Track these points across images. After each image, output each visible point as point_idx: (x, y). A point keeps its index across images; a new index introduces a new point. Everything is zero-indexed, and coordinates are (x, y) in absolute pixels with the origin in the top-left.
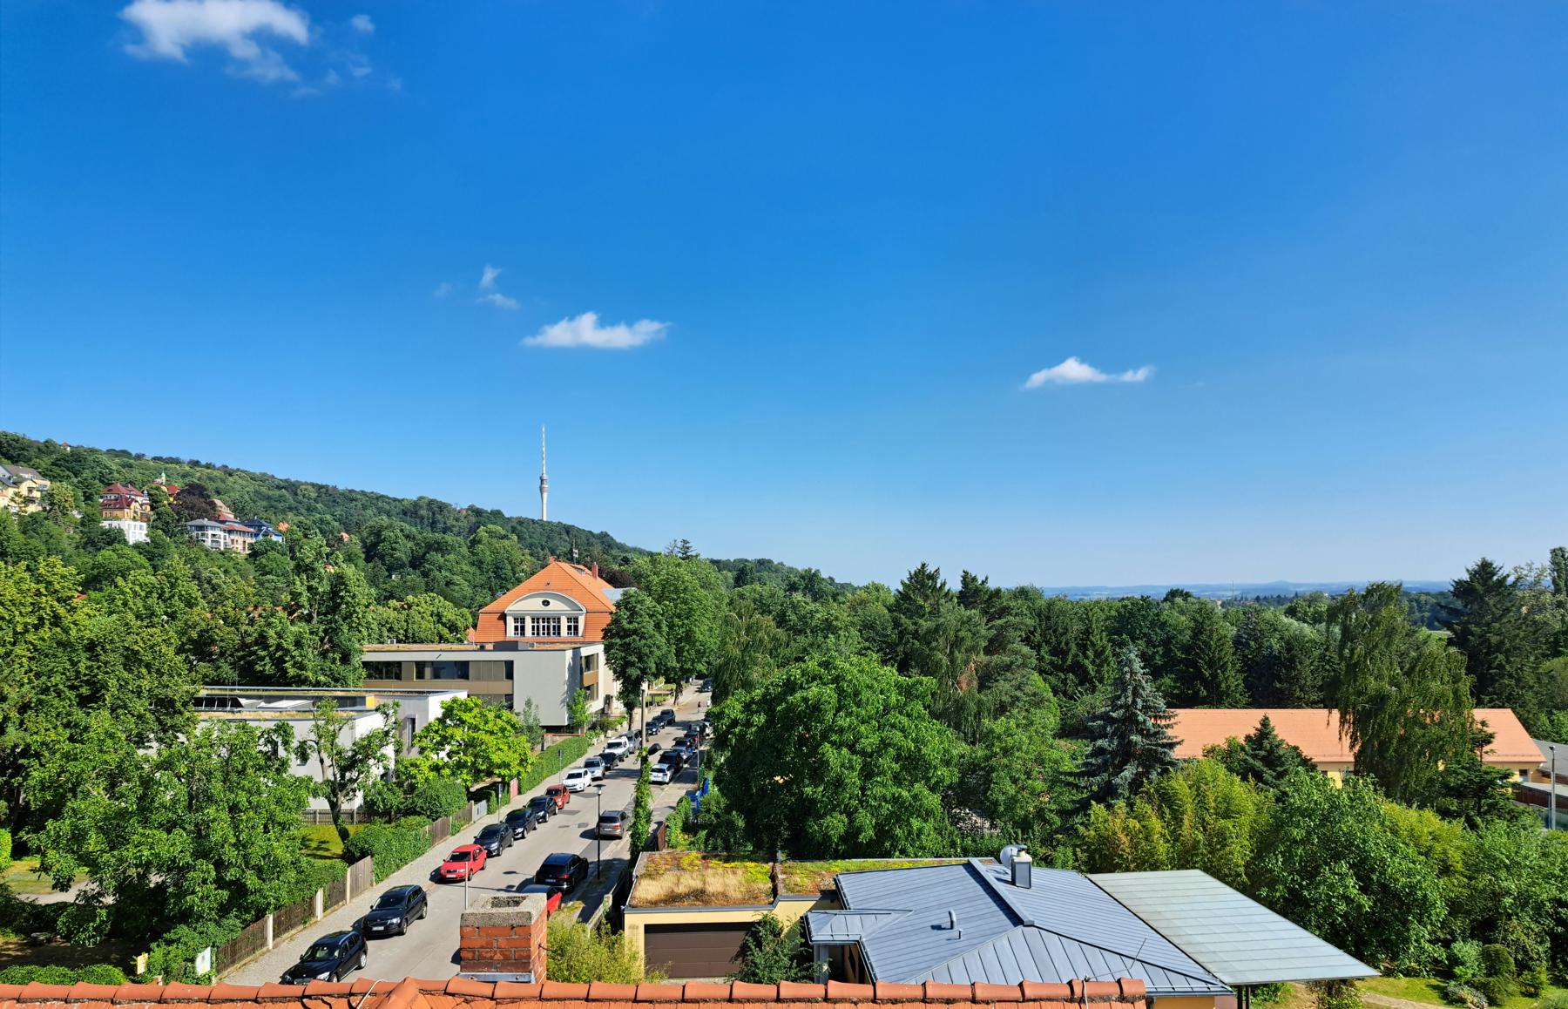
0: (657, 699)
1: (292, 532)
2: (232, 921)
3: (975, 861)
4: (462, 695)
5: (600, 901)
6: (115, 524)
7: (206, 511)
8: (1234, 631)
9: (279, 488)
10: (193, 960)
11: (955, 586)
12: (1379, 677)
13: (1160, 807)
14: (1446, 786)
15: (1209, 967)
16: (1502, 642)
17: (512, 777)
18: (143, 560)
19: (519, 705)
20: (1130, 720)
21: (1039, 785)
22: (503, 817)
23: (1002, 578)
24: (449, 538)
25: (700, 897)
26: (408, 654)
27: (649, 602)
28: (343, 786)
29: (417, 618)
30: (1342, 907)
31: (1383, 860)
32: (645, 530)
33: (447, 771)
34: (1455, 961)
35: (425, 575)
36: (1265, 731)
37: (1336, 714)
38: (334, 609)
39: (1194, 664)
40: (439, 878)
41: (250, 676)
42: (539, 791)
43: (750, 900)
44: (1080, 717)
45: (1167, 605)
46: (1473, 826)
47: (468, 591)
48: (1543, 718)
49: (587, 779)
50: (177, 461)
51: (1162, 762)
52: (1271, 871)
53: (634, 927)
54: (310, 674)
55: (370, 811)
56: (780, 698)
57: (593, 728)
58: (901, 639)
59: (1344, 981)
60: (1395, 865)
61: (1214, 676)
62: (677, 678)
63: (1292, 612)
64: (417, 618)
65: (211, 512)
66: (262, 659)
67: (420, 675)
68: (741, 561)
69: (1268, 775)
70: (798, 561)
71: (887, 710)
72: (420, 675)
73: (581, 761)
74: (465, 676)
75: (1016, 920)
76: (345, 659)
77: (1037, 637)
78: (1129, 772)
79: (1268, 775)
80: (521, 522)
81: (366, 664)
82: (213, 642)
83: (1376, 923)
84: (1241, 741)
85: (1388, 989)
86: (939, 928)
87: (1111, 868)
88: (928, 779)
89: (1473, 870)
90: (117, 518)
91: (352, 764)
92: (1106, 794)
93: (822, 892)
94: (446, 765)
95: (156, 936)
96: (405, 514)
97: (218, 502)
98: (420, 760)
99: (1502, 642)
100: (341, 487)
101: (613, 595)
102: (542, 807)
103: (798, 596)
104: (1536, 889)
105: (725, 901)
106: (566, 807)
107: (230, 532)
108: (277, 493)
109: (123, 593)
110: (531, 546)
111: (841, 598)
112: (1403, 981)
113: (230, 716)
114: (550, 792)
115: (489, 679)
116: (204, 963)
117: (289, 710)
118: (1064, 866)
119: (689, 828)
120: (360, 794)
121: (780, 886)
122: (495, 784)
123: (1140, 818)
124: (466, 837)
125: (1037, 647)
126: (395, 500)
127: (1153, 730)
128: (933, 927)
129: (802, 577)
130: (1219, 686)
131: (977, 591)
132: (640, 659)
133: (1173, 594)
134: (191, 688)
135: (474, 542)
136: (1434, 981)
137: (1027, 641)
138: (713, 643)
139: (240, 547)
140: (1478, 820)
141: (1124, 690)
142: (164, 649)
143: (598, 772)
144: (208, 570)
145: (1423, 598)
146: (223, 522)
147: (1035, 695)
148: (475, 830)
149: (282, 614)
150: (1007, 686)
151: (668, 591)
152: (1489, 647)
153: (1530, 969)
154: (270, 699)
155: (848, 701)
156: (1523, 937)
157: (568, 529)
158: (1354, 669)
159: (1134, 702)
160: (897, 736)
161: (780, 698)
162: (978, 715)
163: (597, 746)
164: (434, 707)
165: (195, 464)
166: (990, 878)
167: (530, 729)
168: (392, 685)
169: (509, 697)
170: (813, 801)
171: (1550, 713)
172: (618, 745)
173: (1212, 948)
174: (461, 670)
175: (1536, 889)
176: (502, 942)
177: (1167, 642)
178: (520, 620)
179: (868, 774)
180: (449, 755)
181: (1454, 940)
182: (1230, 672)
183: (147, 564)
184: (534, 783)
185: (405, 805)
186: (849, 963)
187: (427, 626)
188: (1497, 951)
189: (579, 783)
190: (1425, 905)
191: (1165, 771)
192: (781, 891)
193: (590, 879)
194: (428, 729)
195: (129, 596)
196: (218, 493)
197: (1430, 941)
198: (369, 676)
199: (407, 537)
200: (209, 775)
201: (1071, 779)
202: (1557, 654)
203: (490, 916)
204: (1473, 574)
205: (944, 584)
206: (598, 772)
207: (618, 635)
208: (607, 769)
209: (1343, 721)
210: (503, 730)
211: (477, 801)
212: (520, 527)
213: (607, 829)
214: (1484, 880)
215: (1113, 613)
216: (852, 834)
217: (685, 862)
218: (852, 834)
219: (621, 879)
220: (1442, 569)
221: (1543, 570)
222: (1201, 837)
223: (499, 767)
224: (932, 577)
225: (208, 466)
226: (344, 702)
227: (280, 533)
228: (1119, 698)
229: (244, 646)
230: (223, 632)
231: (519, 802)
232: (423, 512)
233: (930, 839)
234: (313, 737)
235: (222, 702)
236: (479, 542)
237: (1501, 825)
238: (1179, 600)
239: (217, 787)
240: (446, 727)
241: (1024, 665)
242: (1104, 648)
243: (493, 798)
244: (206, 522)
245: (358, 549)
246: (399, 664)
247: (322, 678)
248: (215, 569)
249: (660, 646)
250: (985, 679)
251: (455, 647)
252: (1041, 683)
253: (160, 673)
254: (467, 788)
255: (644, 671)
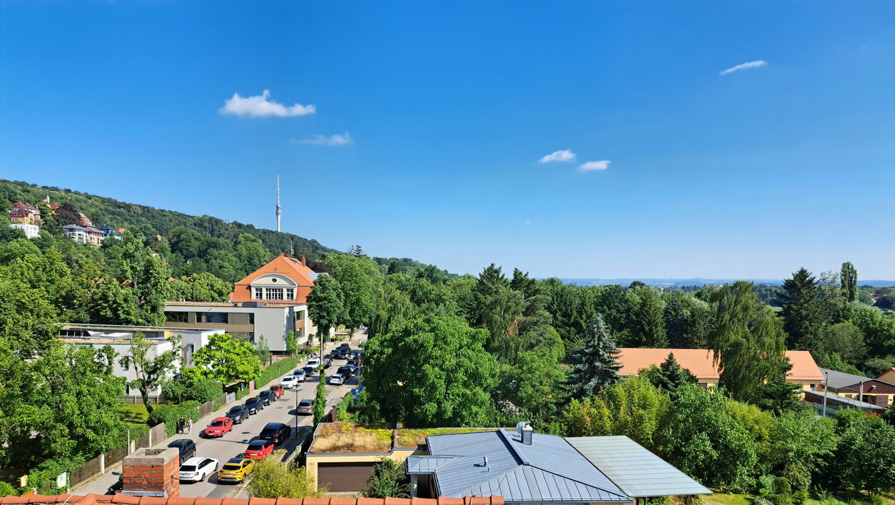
0: (339, 337)
1: (127, 234)
2: (79, 457)
3: (503, 430)
4: (221, 332)
5: (294, 449)
6: (19, 226)
7: (74, 220)
8: (664, 305)
9: (119, 207)
10: (55, 479)
11: (510, 277)
12: (737, 333)
13: (608, 402)
14: (765, 393)
15: (622, 487)
16: (808, 315)
17: (250, 380)
18: (36, 248)
19: (257, 339)
20: (595, 355)
21: (547, 389)
22: (244, 402)
23: (537, 272)
24: (222, 240)
25: (350, 448)
26: (193, 308)
27: (333, 281)
28: (149, 383)
29: (199, 287)
30: (702, 457)
31: (726, 432)
32: (336, 240)
33: (211, 376)
34: (760, 485)
35: (207, 261)
36: (670, 362)
37: (712, 352)
38: (147, 280)
39: (640, 323)
40: (204, 435)
41: (97, 318)
42: (266, 388)
43: (378, 449)
44: (569, 350)
45: (631, 290)
46: (778, 415)
47: (233, 272)
48: (827, 356)
49: (295, 382)
50: (56, 189)
51: (612, 378)
52: (666, 437)
53: (311, 464)
54: (133, 318)
55: (166, 397)
56: (401, 339)
57: (301, 353)
58: (478, 306)
59: (693, 496)
60: (732, 435)
61: (651, 330)
62: (352, 326)
63: (699, 295)
64: (199, 287)
65: (77, 220)
66: (105, 308)
67: (199, 320)
68: (393, 259)
69: (671, 385)
70: (424, 258)
71: (461, 348)
72: (199, 320)
73: (292, 372)
74: (226, 321)
75: (520, 461)
76: (154, 309)
77: (555, 307)
78: (593, 382)
79: (671, 385)
80: (265, 232)
81: (166, 313)
82: (75, 297)
83: (721, 465)
84: (659, 367)
85: (724, 500)
86: (478, 465)
87: (581, 434)
88: (481, 385)
89: (774, 438)
90: (20, 223)
91: (154, 370)
92: (580, 395)
93: (419, 446)
94: (211, 372)
95: (34, 465)
96: (195, 225)
97: (82, 215)
98: (195, 369)
99: (808, 315)
100: (157, 208)
101: (313, 276)
102: (267, 397)
103: (424, 281)
104: (807, 448)
105: (364, 450)
106: (282, 397)
107: (89, 233)
108: (118, 210)
109: (21, 267)
110: (270, 247)
111: (448, 283)
112: (732, 496)
113: (83, 341)
114: (272, 388)
115: (240, 323)
116: (62, 481)
117: (119, 341)
118: (554, 433)
119: (350, 410)
120: (159, 387)
121: (396, 442)
122: (240, 383)
123: (598, 407)
124: (221, 413)
125: (554, 313)
126: (189, 216)
127: (608, 360)
128: (475, 465)
129: (426, 270)
130: (653, 336)
131: (522, 280)
132: (328, 314)
133: (635, 284)
134: (59, 324)
135: (236, 243)
136: (748, 496)
137: (548, 308)
138: (372, 306)
139: (96, 242)
140: (781, 411)
141: (593, 337)
142: (41, 301)
143: (302, 378)
144: (76, 255)
145: (774, 289)
146: (85, 227)
147: (550, 339)
148: (227, 409)
149: (115, 282)
150: (535, 334)
151: (347, 275)
152: (801, 317)
153: (798, 489)
154: (107, 332)
155: (440, 342)
156: (797, 474)
157: (292, 237)
158: (722, 328)
159: (598, 344)
160: (467, 361)
161: (401, 339)
162: (517, 350)
163: (303, 363)
164: (204, 339)
165: (68, 191)
166: (509, 439)
167: (263, 353)
168: (182, 325)
169: (252, 335)
170: (419, 397)
171: (830, 354)
172: (314, 363)
173: (625, 477)
174: (224, 318)
175: (807, 448)
176: (147, 474)
177: (628, 311)
178: (259, 290)
179: (449, 382)
180: (213, 366)
181: (761, 475)
182: (660, 328)
183: (38, 250)
184: (264, 383)
185: (185, 393)
186: (427, 487)
187: (204, 291)
188: (782, 481)
189: (290, 384)
190: (746, 455)
191: (613, 382)
192: (396, 445)
193: (292, 437)
194: (200, 351)
195: (25, 269)
196: (82, 209)
197: (748, 475)
198: (169, 320)
199: (196, 239)
200: (63, 375)
201: (562, 386)
202: (838, 322)
203: (140, 460)
204: (796, 276)
205: (503, 276)
206: (302, 378)
207: (315, 299)
208: (307, 376)
209: (716, 356)
210: (244, 353)
211: (229, 392)
212: (265, 235)
213: (304, 409)
214: (779, 444)
215: (600, 294)
216: (440, 414)
217: (344, 428)
218: (440, 414)
219: (306, 437)
220: (779, 273)
221: (837, 275)
222: (629, 419)
223: (242, 374)
224: (497, 272)
225: (76, 193)
226: (149, 334)
227: (119, 235)
228: (590, 341)
229: (93, 300)
230: (80, 292)
231: (254, 393)
232: (206, 224)
233: (482, 417)
234: (131, 354)
235: (78, 333)
236: (240, 243)
237: (791, 414)
238: (638, 287)
239: (69, 382)
240: (210, 350)
241: (545, 323)
242: (592, 313)
243: (239, 391)
244: (74, 226)
245: (166, 245)
246: (187, 313)
247: (140, 320)
248: (81, 255)
249: (339, 306)
250: (523, 329)
251: (220, 304)
252: (555, 333)
253: (38, 316)
254: (224, 385)
255: (330, 322)
